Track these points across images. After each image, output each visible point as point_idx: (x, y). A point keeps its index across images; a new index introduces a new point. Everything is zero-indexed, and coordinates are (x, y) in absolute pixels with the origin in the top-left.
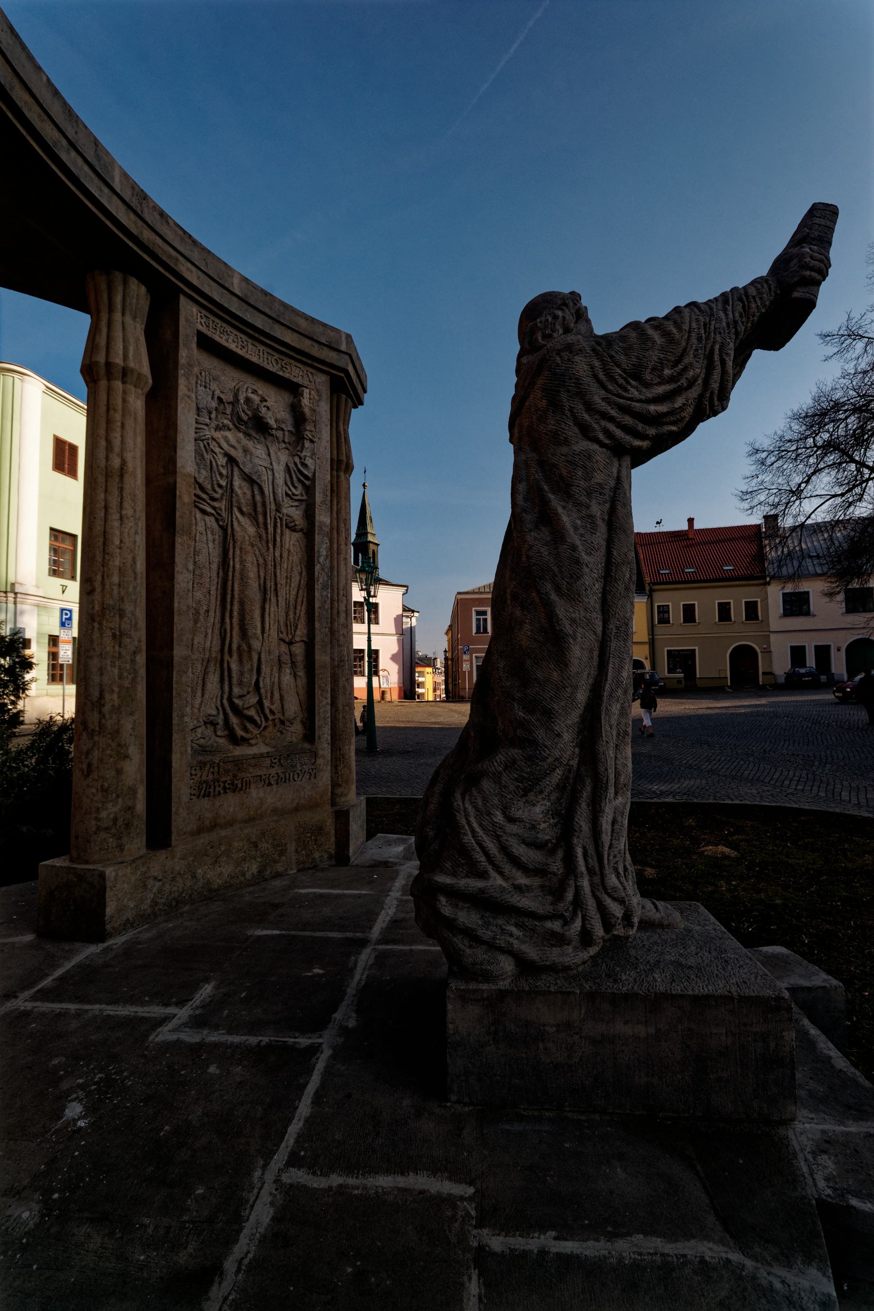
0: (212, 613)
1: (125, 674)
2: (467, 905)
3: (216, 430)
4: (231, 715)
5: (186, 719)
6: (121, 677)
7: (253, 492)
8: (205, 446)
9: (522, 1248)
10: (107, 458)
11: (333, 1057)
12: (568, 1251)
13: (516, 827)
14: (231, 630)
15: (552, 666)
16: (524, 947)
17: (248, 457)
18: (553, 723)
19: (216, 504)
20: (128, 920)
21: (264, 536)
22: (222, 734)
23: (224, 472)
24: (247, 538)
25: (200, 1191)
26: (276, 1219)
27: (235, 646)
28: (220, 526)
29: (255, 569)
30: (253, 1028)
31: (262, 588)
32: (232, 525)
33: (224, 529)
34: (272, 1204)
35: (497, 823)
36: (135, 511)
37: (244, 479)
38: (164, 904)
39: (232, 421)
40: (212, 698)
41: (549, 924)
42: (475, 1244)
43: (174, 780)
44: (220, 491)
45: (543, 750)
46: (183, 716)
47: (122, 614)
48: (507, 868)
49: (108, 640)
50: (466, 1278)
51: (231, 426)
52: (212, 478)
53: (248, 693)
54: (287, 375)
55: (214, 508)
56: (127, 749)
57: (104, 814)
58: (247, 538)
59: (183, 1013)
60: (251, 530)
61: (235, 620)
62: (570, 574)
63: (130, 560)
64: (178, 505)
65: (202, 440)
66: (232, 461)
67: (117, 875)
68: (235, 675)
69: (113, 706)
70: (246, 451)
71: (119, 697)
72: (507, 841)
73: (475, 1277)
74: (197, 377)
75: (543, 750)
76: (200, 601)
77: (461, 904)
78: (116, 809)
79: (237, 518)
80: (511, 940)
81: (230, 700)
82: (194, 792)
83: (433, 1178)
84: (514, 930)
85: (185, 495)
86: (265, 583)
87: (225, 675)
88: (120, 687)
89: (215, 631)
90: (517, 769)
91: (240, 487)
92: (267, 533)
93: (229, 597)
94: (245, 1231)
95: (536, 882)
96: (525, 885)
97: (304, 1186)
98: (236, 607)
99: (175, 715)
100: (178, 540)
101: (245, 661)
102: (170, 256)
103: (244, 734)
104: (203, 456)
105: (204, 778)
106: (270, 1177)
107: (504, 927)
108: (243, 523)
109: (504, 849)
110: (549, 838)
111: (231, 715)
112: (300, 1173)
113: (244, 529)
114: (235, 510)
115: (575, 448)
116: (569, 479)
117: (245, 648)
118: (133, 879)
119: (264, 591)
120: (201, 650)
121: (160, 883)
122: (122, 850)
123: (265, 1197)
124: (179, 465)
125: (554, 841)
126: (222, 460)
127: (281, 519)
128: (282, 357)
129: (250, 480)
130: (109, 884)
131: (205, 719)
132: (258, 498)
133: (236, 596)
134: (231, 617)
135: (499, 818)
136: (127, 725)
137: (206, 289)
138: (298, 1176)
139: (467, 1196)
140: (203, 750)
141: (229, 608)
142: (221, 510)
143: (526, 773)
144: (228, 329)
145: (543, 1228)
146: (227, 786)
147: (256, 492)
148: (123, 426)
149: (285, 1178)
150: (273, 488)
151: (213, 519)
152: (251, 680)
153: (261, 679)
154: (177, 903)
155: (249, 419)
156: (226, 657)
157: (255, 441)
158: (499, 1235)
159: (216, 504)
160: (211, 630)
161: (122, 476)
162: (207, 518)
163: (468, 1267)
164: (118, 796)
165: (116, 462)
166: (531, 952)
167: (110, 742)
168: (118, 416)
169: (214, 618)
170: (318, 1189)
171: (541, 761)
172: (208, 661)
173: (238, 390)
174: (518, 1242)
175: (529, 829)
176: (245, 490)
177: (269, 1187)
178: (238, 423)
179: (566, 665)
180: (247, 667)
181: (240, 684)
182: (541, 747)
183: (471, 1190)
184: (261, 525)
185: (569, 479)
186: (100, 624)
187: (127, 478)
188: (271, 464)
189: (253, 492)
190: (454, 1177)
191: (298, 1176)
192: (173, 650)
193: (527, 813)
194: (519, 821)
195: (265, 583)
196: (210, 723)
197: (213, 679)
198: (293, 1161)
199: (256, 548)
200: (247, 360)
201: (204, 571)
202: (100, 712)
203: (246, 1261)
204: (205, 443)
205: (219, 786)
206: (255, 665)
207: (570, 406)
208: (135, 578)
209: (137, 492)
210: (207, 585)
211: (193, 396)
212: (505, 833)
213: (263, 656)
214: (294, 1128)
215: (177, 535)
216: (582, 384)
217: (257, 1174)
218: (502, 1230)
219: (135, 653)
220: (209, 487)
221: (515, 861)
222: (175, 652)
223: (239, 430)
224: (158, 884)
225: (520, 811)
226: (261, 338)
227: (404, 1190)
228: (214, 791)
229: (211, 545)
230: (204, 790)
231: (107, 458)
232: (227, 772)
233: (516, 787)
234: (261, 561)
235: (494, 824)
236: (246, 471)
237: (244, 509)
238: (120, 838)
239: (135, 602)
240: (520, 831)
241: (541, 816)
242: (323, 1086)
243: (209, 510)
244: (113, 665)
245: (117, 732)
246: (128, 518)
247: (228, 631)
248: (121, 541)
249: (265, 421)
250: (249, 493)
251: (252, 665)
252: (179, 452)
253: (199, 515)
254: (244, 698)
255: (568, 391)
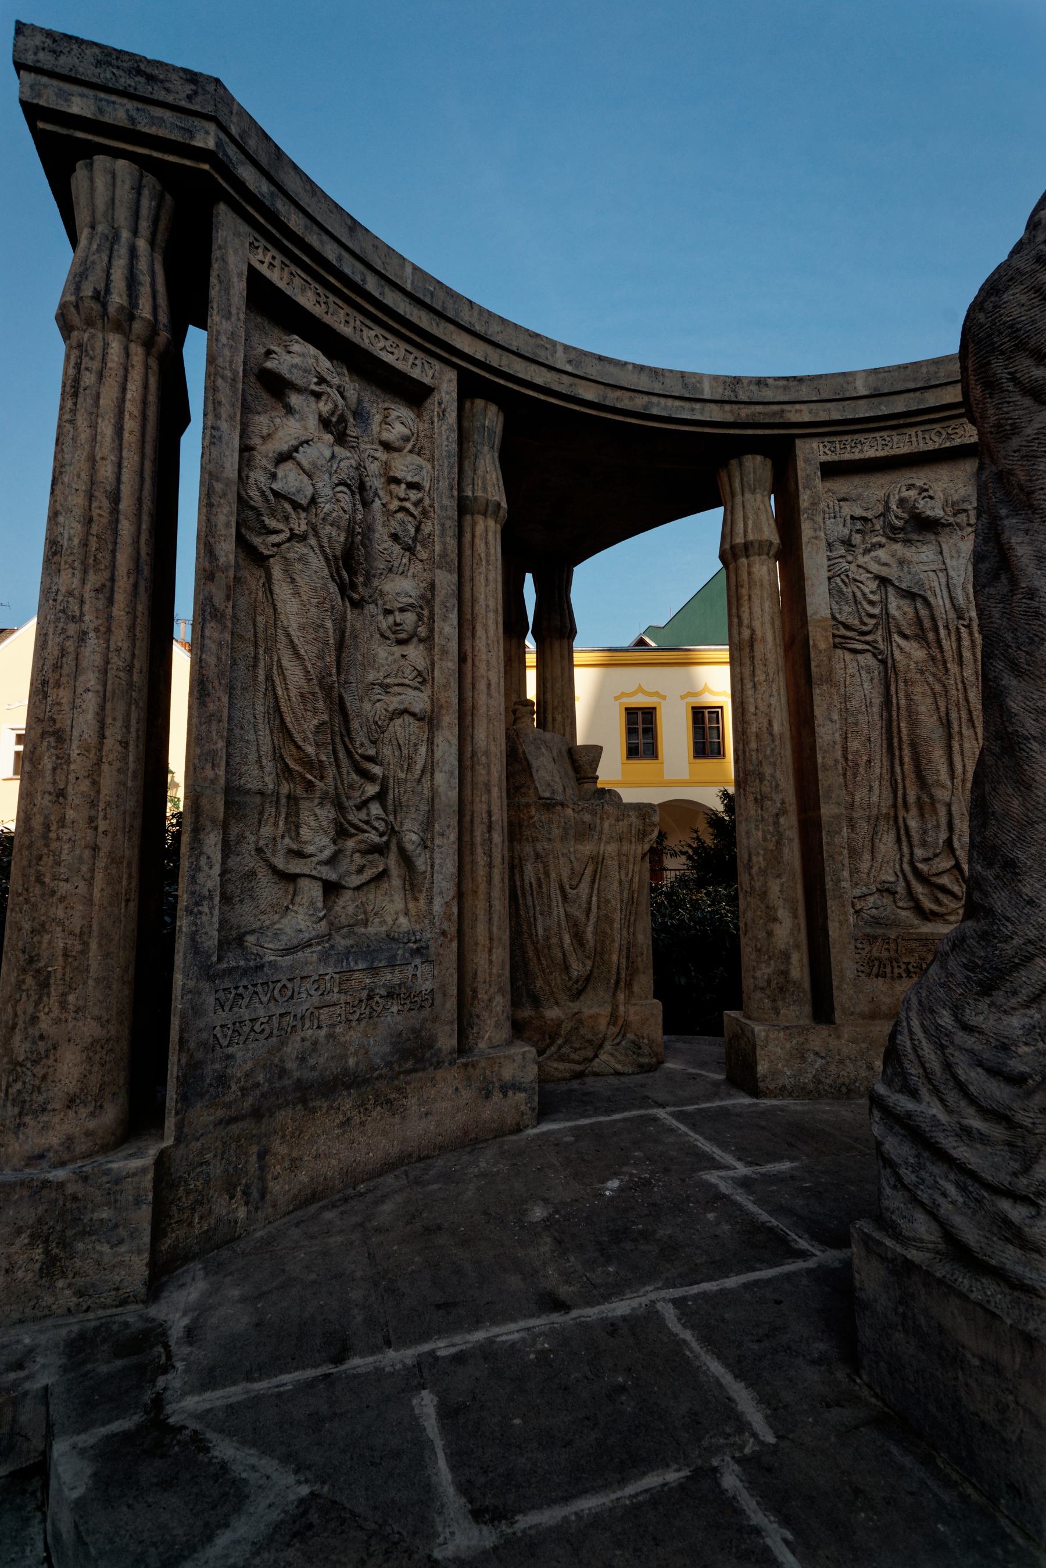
0: (877, 764)
1: (769, 837)
2: (902, 1132)
3: (864, 554)
4: (914, 883)
5: (843, 884)
6: (765, 839)
7: (916, 608)
8: (843, 581)
9: (745, 1508)
10: (739, 633)
11: (809, 1271)
12: (781, 1559)
13: (973, 1039)
14: (903, 779)
15: (1010, 791)
16: (957, 1220)
17: (906, 569)
18: (1020, 881)
19: (868, 638)
20: (784, 1086)
21: (939, 656)
22: (905, 905)
23: (875, 598)
24: (913, 665)
25: (611, 1269)
26: (624, 1318)
27: (911, 798)
28: (879, 660)
29: (929, 701)
30: (778, 1210)
31: (944, 721)
32: (892, 655)
33: (883, 662)
34: (633, 1309)
35: (942, 1026)
36: (767, 675)
37: (903, 597)
38: (831, 1086)
39: (885, 535)
40: (888, 862)
41: (1005, 1205)
42: (715, 1464)
43: (834, 951)
44: (873, 622)
45: (1003, 925)
46: (839, 881)
47: (761, 778)
48: (952, 1097)
49: (751, 804)
50: (675, 1466)
51: (883, 540)
52: (858, 611)
53: (936, 856)
54: (957, 442)
55: (867, 643)
56: (776, 912)
57: (759, 974)
58: (913, 665)
59: (742, 1170)
60: (918, 653)
61: (908, 766)
62: (1030, 638)
63: (766, 724)
64: (812, 655)
65: (839, 575)
66: (884, 581)
67: (767, 1036)
68: (913, 833)
69: (760, 868)
70: (901, 562)
71: (764, 860)
72: (953, 1055)
73: (682, 1474)
74: (824, 512)
75: (1003, 925)
76: (857, 752)
77: (897, 1127)
78: (769, 970)
79: (899, 646)
80: (940, 1200)
81: (912, 863)
82: (862, 968)
83: (754, 1403)
84: (952, 1190)
85: (820, 639)
86: (947, 714)
87: (903, 835)
88: (765, 849)
89: (884, 783)
90: (965, 950)
91: (899, 608)
92: (942, 652)
93: (896, 740)
94: (602, 1307)
95: (997, 1132)
96: (978, 1130)
97: (664, 1319)
98: (907, 752)
99: (828, 879)
100: (816, 691)
101: (927, 816)
102: (774, 414)
103: (934, 907)
104: (841, 592)
105: (875, 954)
106: (652, 1296)
107: (938, 1179)
108: (907, 649)
109: (948, 1067)
110: (1028, 1070)
111: (914, 883)
112: (672, 1311)
113: (909, 656)
114: (895, 636)
115: (1029, 431)
116: (1029, 484)
117: (926, 800)
118: (788, 1045)
119: (946, 724)
120: (865, 806)
121: (823, 1061)
122: (778, 1014)
123: (635, 1303)
124: (809, 612)
125: (1038, 1078)
126: (874, 585)
127: (968, 627)
128: (944, 424)
129: (909, 595)
130: (759, 1043)
131: (879, 886)
132: (923, 612)
133: (905, 738)
134: (902, 764)
135: (946, 1019)
136: (775, 888)
137: (823, 417)
138: (670, 1314)
139: (762, 1438)
140: (876, 921)
141: (897, 753)
142: (877, 642)
143: (980, 958)
144: (861, 437)
145: (786, 1521)
146: (912, 970)
147: (919, 605)
148: (750, 597)
149: (659, 1306)
150: (949, 591)
151: (869, 656)
152: (938, 839)
153: (955, 838)
154: (849, 1091)
155: (906, 522)
156: (901, 813)
157: (918, 544)
158: (741, 1481)
159: (868, 638)
160: (877, 783)
161: (752, 646)
162: (860, 657)
163: (688, 1466)
164: (770, 958)
165: (746, 633)
166: (971, 1234)
167: (759, 903)
168: (744, 591)
169: (879, 767)
170: (669, 1329)
171: (1000, 942)
172: (878, 818)
173: (888, 496)
174: (749, 1503)
175: (996, 1047)
176: (906, 609)
177: (644, 1300)
178: (893, 533)
179: (1029, 788)
180: (931, 824)
181: (924, 844)
182: (1000, 920)
183: (771, 1439)
184: (933, 644)
185: (1029, 484)
186: (744, 790)
187: (758, 648)
188: (944, 563)
189: (916, 608)
190: (772, 1420)
191: (670, 1314)
192: (819, 808)
193: (991, 1022)
194: (979, 1032)
195: (947, 714)
196: (887, 890)
197: (887, 842)
198: (678, 1303)
199: (927, 674)
200: (894, 456)
201: (860, 717)
202: (750, 874)
203: (583, 1319)
204: (842, 576)
205: (899, 967)
206: (943, 821)
207: (1009, 373)
208: (773, 741)
209: (769, 655)
210: (865, 732)
211: (822, 534)
212: (952, 1043)
213: (955, 808)
214: (706, 1286)
215: (814, 686)
216: (1019, 330)
217: (648, 1288)
218: (750, 1483)
219: (777, 815)
220: (857, 622)
221: (962, 1088)
222: (822, 811)
223: (895, 541)
224: (820, 1062)
225: (980, 1015)
226: (909, 420)
227: (720, 1385)
228: (892, 972)
229: (866, 685)
230: (875, 967)
231: (739, 633)
232: (911, 951)
233: (966, 977)
234: (937, 687)
235: (938, 1027)
236: (904, 586)
237: (907, 632)
238: (774, 1001)
239: (775, 764)
240: (977, 1047)
241: (1020, 1032)
242: (768, 1282)
243: (860, 647)
244: (757, 828)
245: (765, 893)
246: (760, 684)
247: (899, 781)
248: (756, 708)
249: (923, 516)
250: (910, 610)
251: (937, 820)
252: (808, 600)
253: (848, 656)
254: (931, 862)
255: (1002, 353)
